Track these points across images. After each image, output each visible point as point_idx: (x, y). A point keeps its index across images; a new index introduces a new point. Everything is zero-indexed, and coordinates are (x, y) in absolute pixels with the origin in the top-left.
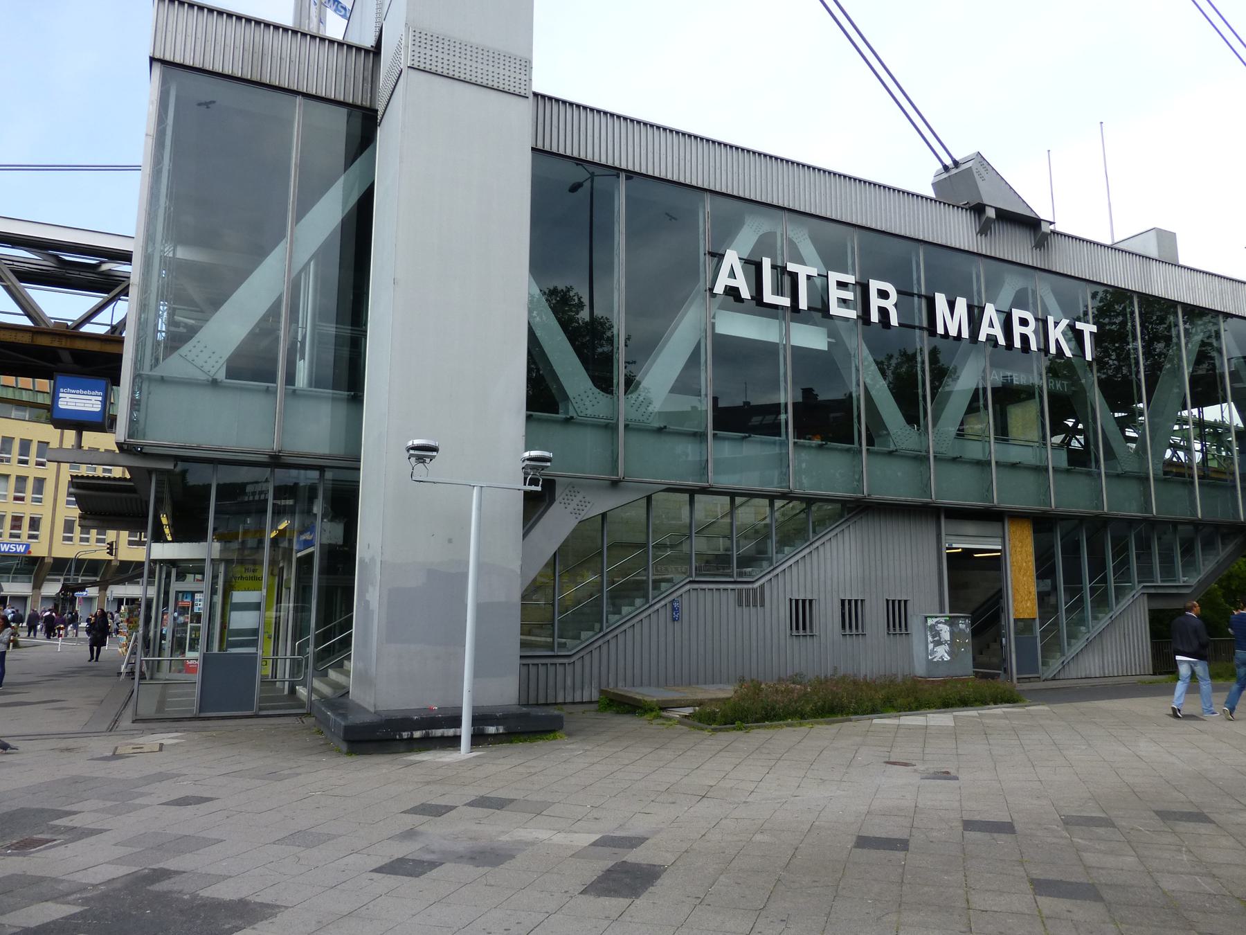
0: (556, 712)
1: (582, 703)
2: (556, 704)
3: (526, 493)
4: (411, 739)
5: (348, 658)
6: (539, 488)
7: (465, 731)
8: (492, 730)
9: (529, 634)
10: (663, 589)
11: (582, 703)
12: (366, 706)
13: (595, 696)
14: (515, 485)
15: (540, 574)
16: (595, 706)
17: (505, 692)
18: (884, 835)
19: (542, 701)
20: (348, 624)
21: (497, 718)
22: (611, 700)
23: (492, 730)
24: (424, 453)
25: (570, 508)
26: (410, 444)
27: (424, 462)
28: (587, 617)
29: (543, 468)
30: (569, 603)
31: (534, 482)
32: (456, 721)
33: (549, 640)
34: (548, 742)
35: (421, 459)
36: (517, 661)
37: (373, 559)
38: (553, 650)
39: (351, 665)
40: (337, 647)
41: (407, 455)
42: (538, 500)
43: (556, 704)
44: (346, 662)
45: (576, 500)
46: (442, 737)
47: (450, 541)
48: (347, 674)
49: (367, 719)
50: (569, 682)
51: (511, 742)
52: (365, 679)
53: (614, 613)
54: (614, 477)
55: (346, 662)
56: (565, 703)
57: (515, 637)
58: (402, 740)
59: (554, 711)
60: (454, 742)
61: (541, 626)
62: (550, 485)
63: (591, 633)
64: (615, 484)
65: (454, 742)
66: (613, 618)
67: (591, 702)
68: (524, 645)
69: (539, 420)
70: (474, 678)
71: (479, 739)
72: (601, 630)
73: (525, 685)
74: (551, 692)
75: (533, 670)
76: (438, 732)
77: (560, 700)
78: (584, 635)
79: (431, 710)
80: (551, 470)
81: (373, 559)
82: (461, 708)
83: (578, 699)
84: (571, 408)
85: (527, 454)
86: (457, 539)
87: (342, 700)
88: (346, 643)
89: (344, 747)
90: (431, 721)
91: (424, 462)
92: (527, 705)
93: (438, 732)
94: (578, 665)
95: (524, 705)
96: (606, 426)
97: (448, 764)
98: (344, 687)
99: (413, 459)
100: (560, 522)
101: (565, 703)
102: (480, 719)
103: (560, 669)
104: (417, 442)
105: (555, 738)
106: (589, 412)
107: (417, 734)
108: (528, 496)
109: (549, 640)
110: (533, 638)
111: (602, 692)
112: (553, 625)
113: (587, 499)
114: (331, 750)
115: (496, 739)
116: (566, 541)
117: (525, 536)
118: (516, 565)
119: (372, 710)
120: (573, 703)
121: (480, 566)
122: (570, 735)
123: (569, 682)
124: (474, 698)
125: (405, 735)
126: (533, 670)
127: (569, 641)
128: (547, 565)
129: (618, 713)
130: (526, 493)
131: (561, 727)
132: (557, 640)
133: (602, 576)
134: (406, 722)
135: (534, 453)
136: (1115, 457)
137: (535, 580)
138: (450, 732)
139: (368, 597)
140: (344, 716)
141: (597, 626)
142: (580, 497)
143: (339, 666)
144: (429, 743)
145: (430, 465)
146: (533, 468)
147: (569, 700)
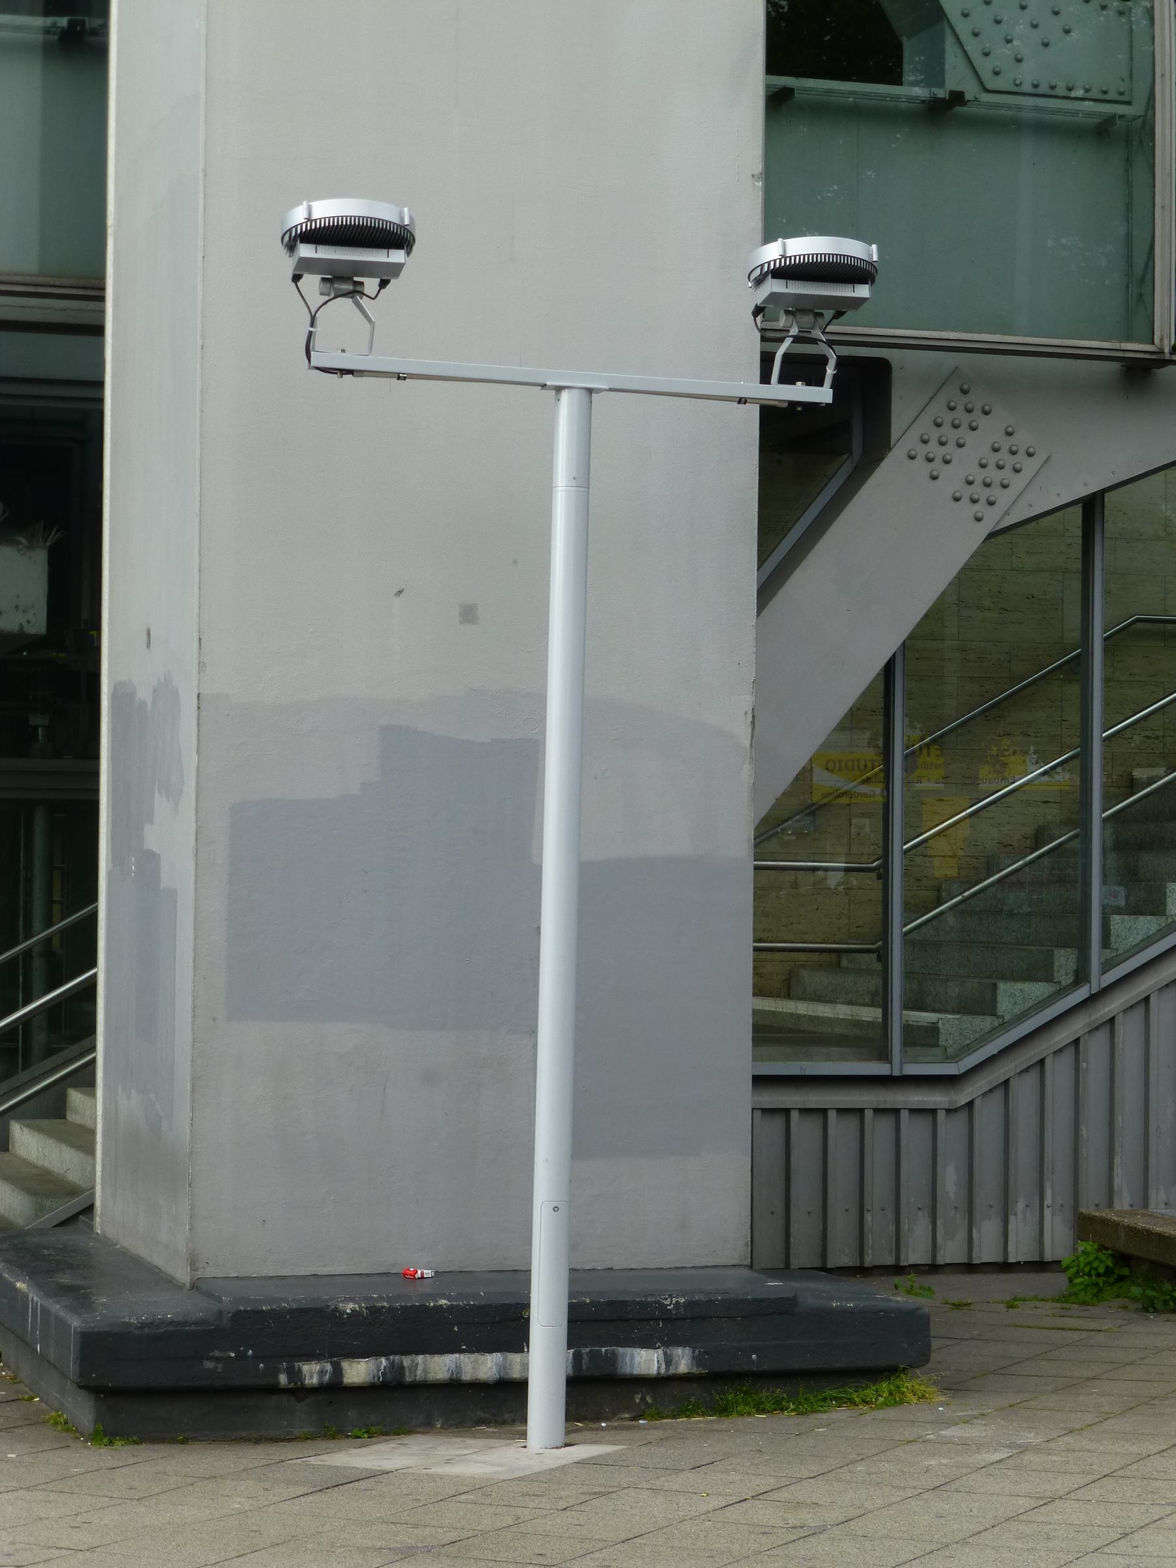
0: (901, 1300)
1: (1005, 1267)
2: (898, 1269)
3: (770, 415)
4: (335, 1389)
5: (85, 1079)
6: (823, 395)
7: (544, 1362)
8: (645, 1361)
9: (787, 993)
10: (1005, 1006)
11: (1005, 1267)
12: (159, 1260)
13: (1058, 1240)
14: (713, 374)
15: (824, 759)
16: (1058, 1282)
17: (697, 1213)
18: (64, 1147)
19: (842, 1256)
20: (80, 947)
21: (668, 1318)
22: (1123, 1258)
23: (645, 1361)
24: (352, 254)
25: (952, 479)
26: (298, 217)
27: (356, 292)
28: (1022, 923)
29: (841, 308)
30: (943, 869)
31: (802, 368)
32: (506, 1326)
33: (871, 1014)
34: (871, 1415)
35: (343, 282)
36: (744, 1097)
37: (165, 690)
38: (884, 1055)
39: (96, 1108)
40: (40, 1038)
41: (288, 265)
42: (817, 449)
43: (898, 1269)
44: (75, 1097)
45: (978, 445)
46: (454, 1386)
47: (468, 614)
48: (83, 1140)
49: (167, 1308)
50: (951, 1179)
51: (723, 1411)
52: (153, 1160)
53: (1135, 910)
54: (1135, 347)
55: (75, 1097)
56: (934, 1268)
57: (736, 1004)
58: (299, 1391)
59: (893, 1296)
60: (501, 1404)
61: (834, 959)
62: (867, 382)
63: (1040, 989)
64: (1138, 374)
65: (501, 1404)
66: (1131, 929)
67: (1040, 1266)
68: (766, 1033)
69: (822, 110)
70: (579, 1163)
71: (595, 1394)
72: (1081, 976)
73: (776, 1190)
74: (878, 1223)
75: (804, 1132)
76: (438, 1367)
77: (915, 1254)
78: (1012, 995)
79: (408, 1277)
80: (873, 320)
81: (165, 690)
82: (523, 1276)
83: (987, 1252)
84: (952, 60)
85: (772, 252)
86: (495, 609)
87: (69, 1237)
88: (74, 1022)
89: (83, 1411)
90: (410, 1324)
91: (356, 292)
92: (785, 1270)
93: (438, 1367)
94: (988, 1117)
95: (772, 1272)
96: (1103, 132)
97: (481, 1487)
98: (72, 1191)
99: (312, 282)
100: (909, 536)
101: (934, 1268)
102: (598, 1320)
103: (914, 1132)
104: (328, 209)
105: (895, 1399)
106: (1027, 75)
107: (358, 1371)
108: (782, 432)
109: (871, 1014)
110: (802, 1008)
111: (1084, 1226)
112: (883, 955)
113: (1023, 439)
114: (35, 1421)
115: (664, 1397)
116: (934, 615)
117: (767, 591)
118: (732, 712)
119: (183, 1275)
120: (970, 1268)
121: (590, 718)
122: (955, 1387)
123: (951, 1179)
124: (574, 1240)
125: (312, 1372)
126: (804, 1132)
127: (949, 1023)
128: (853, 720)
129: (1148, 1307)
130: (770, 415)
131: (922, 1358)
132: (900, 1016)
133: (1084, 757)
134: (311, 1325)
135: (804, 247)
136: (572, 1271)
137: (804, 777)
138: (485, 1366)
139: (152, 839)
140: (79, 1297)
141: (1064, 961)
142: (991, 430)
143: (51, 1111)
144: (400, 1407)
145: (384, 305)
146: (798, 308)
147: (951, 1252)
